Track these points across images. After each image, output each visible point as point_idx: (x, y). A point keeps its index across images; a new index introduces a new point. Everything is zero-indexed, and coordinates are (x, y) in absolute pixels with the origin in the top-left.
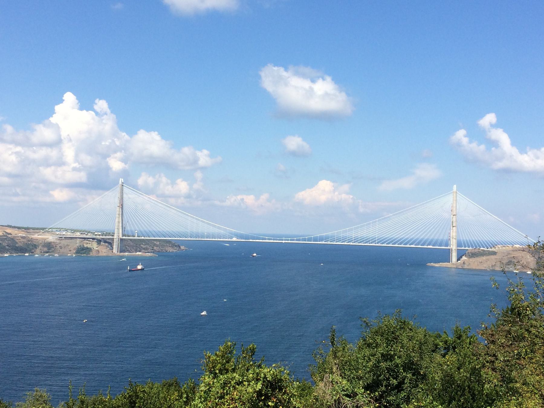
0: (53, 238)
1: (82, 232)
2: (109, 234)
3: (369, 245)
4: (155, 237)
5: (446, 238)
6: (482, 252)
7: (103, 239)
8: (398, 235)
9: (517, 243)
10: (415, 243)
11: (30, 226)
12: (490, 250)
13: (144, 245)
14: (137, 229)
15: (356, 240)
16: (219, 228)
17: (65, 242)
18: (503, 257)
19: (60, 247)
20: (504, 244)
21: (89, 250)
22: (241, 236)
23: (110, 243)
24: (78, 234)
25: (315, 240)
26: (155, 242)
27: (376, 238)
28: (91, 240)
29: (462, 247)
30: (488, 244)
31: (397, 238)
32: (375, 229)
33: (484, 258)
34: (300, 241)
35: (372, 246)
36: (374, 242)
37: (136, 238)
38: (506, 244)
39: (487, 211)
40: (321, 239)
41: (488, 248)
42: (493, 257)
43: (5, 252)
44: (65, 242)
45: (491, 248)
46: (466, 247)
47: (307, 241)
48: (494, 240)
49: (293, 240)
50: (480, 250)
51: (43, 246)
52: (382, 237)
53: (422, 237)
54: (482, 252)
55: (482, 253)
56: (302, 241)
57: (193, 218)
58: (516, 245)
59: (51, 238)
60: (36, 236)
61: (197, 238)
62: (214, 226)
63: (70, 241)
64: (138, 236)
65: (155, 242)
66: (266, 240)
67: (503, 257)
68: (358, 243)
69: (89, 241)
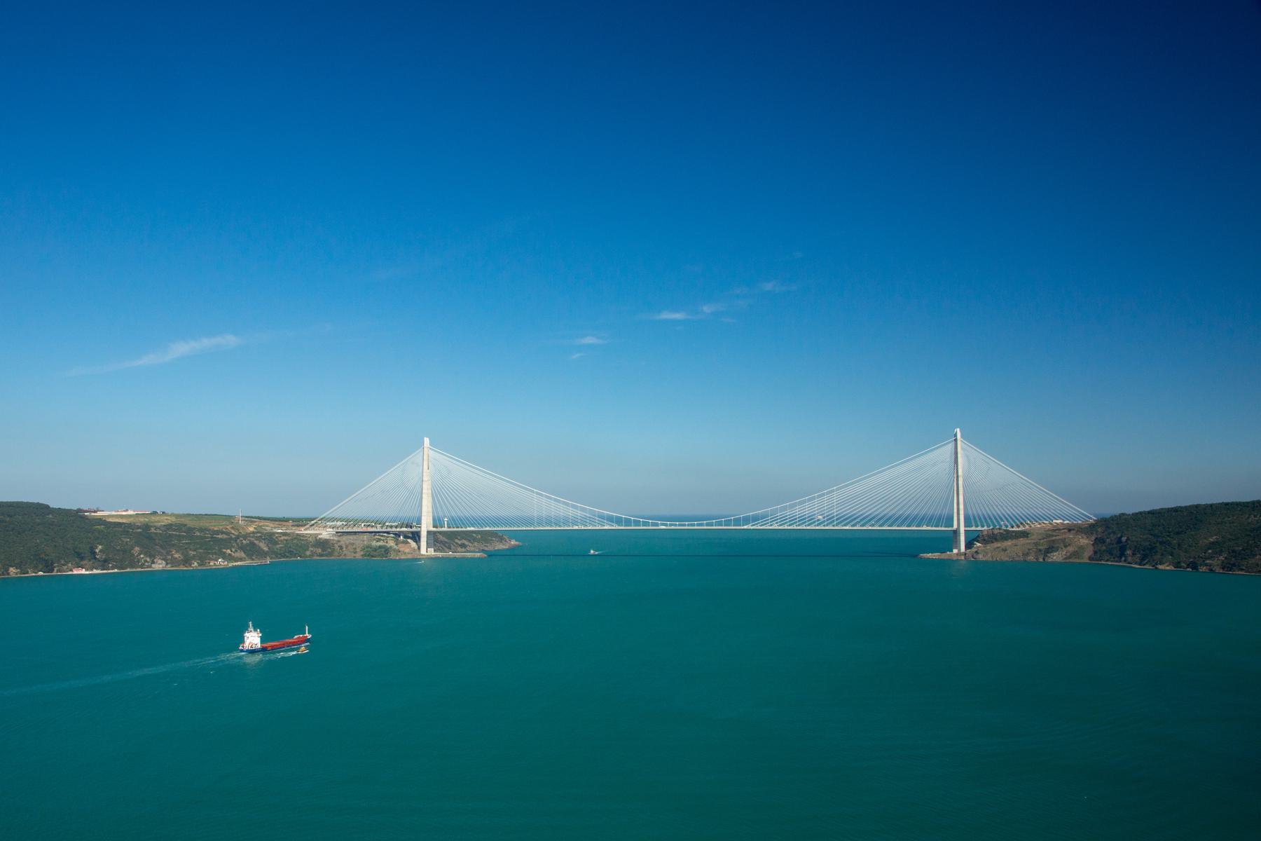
2: (938, 520)
4: (458, 527)
5: (946, 512)
7: (403, 532)
11: (287, 516)
17: (345, 540)
18: (1040, 540)
20: (1036, 518)
21: (387, 550)
22: (619, 521)
23: (416, 536)
24: (362, 528)
25: (737, 521)
27: (833, 517)
29: (972, 526)
31: (894, 515)
32: (832, 507)
34: (965, 526)
37: (445, 529)
40: (747, 520)
41: (1013, 527)
42: (1022, 541)
44: (345, 540)
45: (1018, 526)
49: (702, 525)
50: (1001, 531)
52: (855, 514)
53: (908, 512)
57: (559, 501)
59: (326, 534)
60: (302, 531)
62: (573, 506)
63: (355, 537)
66: (649, 526)
67: (1040, 540)
69: (382, 536)
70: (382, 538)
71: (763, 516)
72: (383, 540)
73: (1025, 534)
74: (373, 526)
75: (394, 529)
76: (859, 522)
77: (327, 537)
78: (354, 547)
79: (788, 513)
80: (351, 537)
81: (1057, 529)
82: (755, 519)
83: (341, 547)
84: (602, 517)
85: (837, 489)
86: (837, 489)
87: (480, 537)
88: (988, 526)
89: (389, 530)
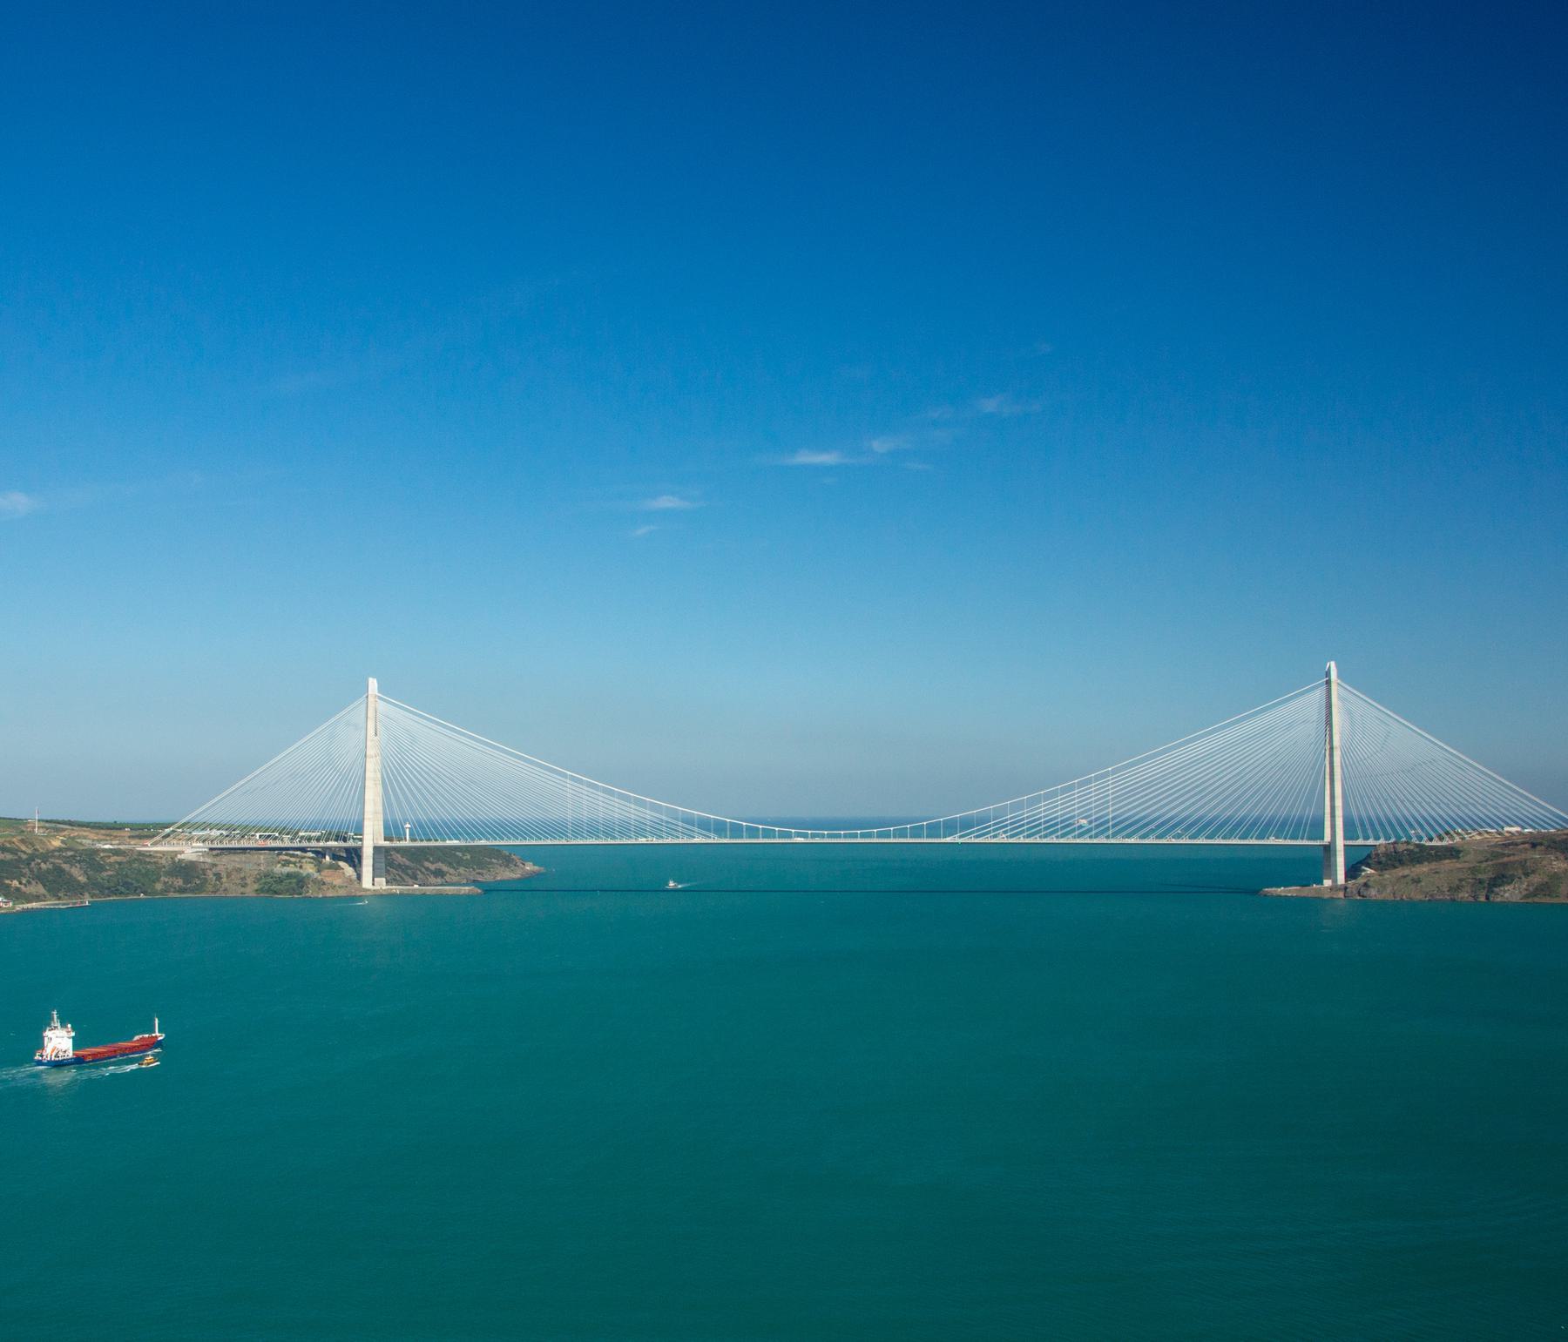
0: (196, 850)
1: (268, 830)
3: (1088, 841)
5: (1310, 812)
6: (1417, 850)
7: (329, 848)
8: (1157, 810)
9: (1512, 820)
10: (1227, 828)
11: (121, 819)
12: (1439, 844)
13: (432, 863)
14: (410, 816)
15: (1034, 829)
16: (654, 808)
17: (227, 862)
19: (215, 875)
20: (1475, 824)
25: (933, 830)
26: (459, 854)
28: (298, 853)
30: (434, 828)
33: (1424, 868)
35: (1006, 843)
36: (1102, 832)
37: (407, 843)
38: (1483, 824)
39: (1442, 745)
40: (950, 827)
42: (1447, 864)
43: (1517, 834)
44: (227, 862)
46: (1357, 839)
47: (779, 838)
48: (1420, 814)
49: (869, 835)
50: (1411, 847)
51: (170, 873)
54: (1417, 850)
55: (1417, 853)
56: (895, 837)
58: (1512, 826)
59: (190, 851)
60: (149, 847)
61: (541, 839)
63: (243, 857)
64: (413, 840)
65: (459, 854)
68: (1057, 837)
69: (293, 856)
70: (293, 859)
71: (982, 820)
72: (294, 863)
73: (1452, 853)
74: (276, 838)
75: (314, 844)
76: (1152, 831)
77: (193, 858)
78: (242, 875)
79: (1026, 813)
80: (237, 858)
81: (1510, 843)
82: (966, 824)
83: (218, 876)
84: (689, 821)
85: (1114, 772)
86: (1114, 772)
87: (469, 857)
88: (1387, 838)
89: (305, 844)
